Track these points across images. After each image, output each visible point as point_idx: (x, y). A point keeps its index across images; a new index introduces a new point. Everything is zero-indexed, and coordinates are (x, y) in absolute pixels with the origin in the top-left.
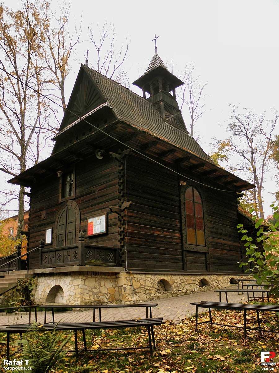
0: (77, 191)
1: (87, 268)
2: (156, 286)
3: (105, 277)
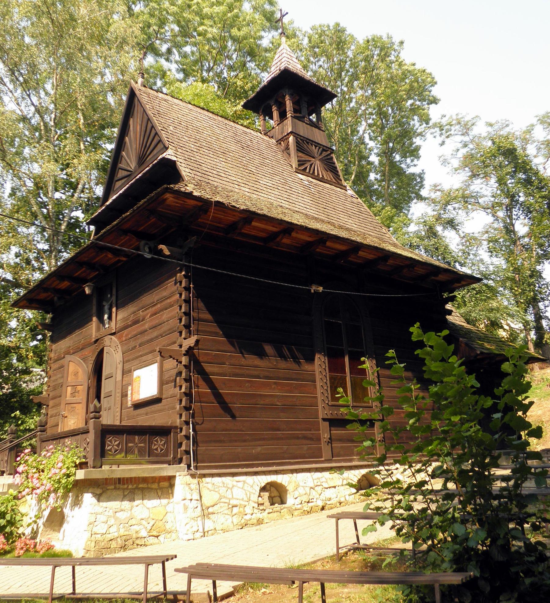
0: (119, 317)
1: (107, 471)
2: (255, 497)
3: (146, 486)
